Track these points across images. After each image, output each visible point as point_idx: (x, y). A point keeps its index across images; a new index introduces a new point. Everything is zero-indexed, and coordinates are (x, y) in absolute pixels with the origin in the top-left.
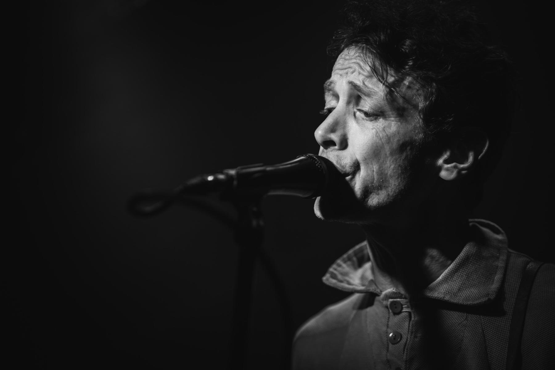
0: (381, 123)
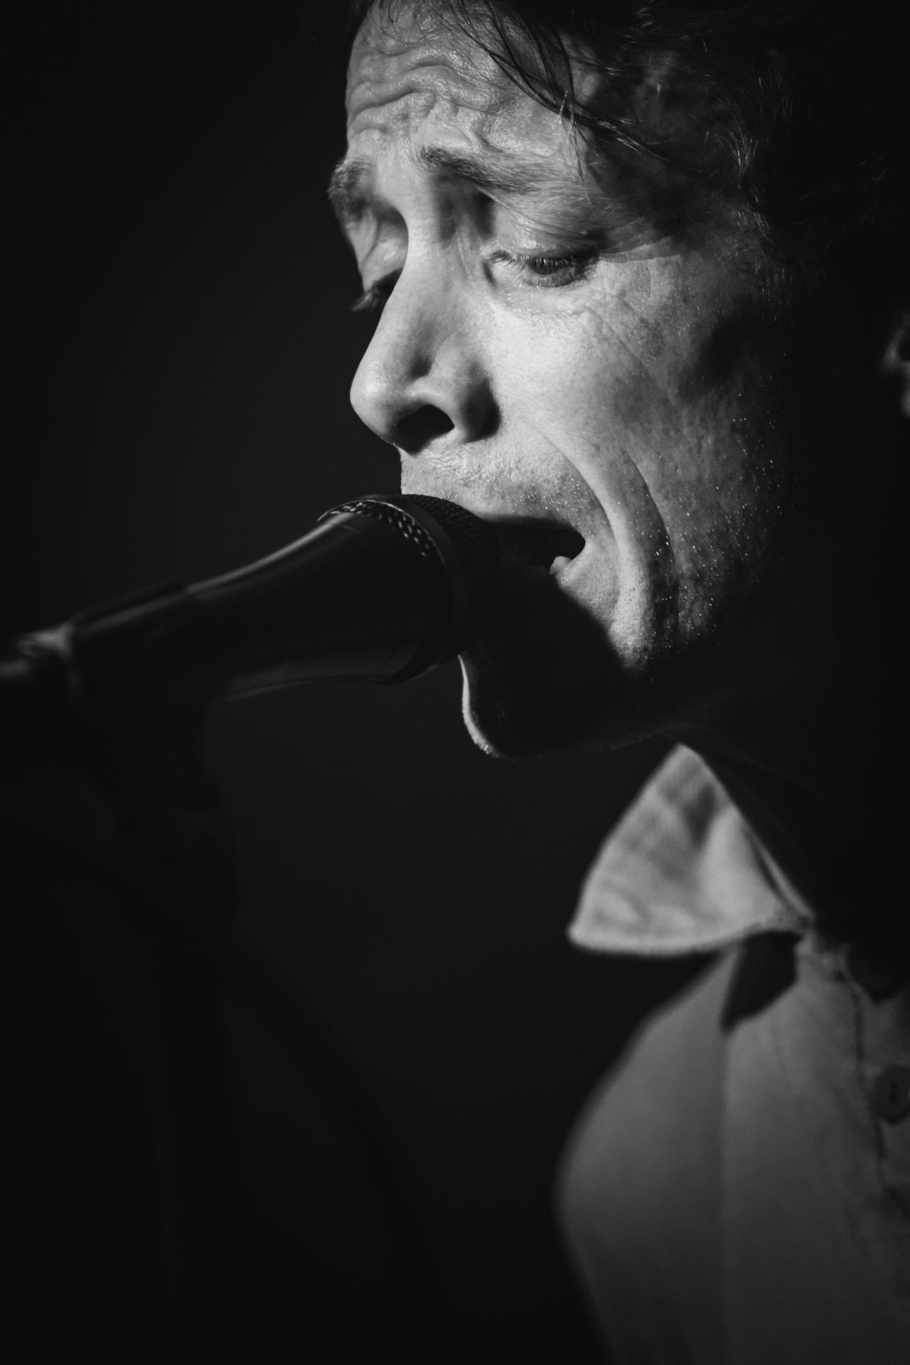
0: (606, 275)
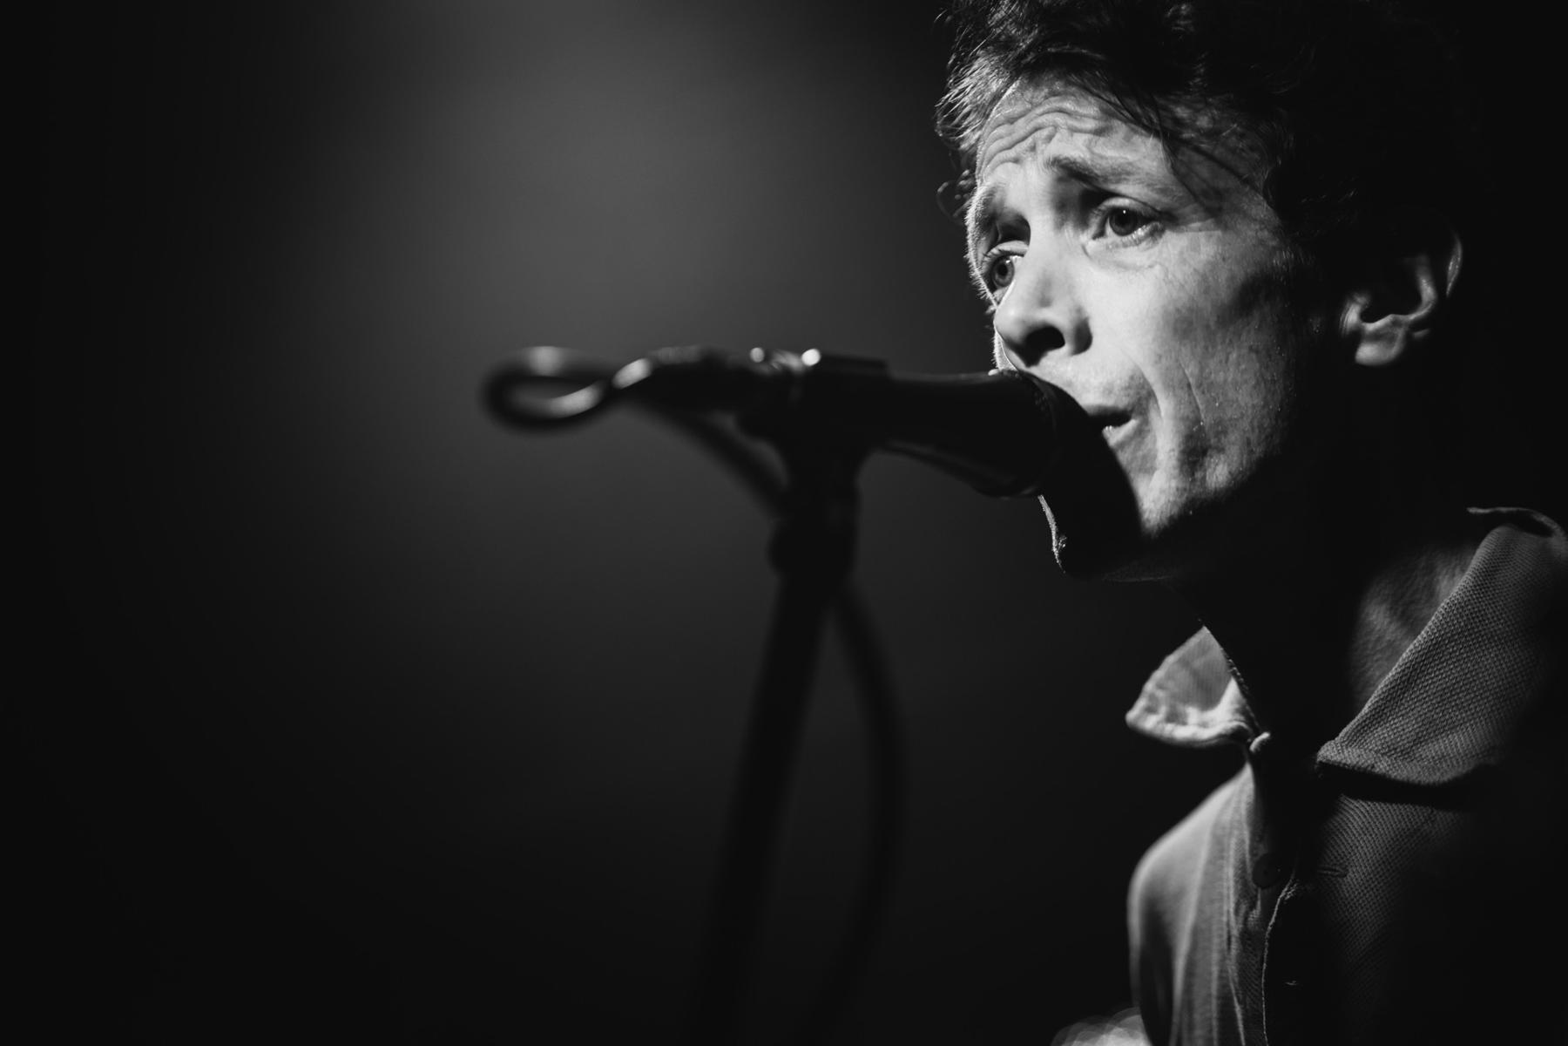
0: (1174, 244)
